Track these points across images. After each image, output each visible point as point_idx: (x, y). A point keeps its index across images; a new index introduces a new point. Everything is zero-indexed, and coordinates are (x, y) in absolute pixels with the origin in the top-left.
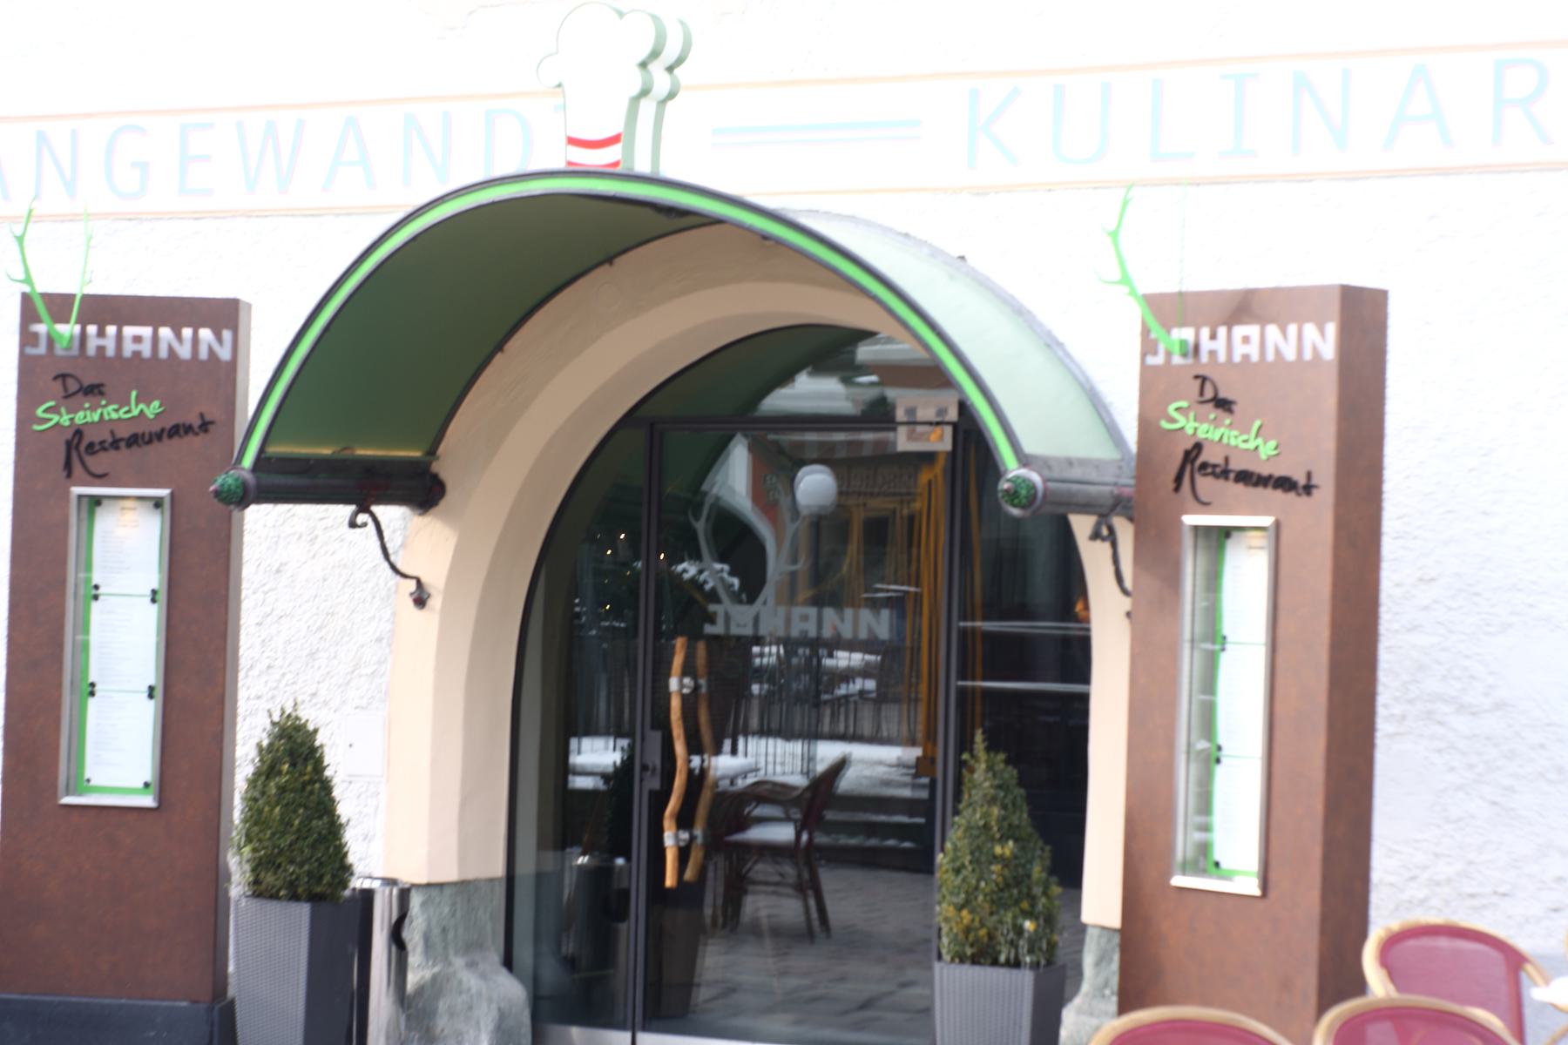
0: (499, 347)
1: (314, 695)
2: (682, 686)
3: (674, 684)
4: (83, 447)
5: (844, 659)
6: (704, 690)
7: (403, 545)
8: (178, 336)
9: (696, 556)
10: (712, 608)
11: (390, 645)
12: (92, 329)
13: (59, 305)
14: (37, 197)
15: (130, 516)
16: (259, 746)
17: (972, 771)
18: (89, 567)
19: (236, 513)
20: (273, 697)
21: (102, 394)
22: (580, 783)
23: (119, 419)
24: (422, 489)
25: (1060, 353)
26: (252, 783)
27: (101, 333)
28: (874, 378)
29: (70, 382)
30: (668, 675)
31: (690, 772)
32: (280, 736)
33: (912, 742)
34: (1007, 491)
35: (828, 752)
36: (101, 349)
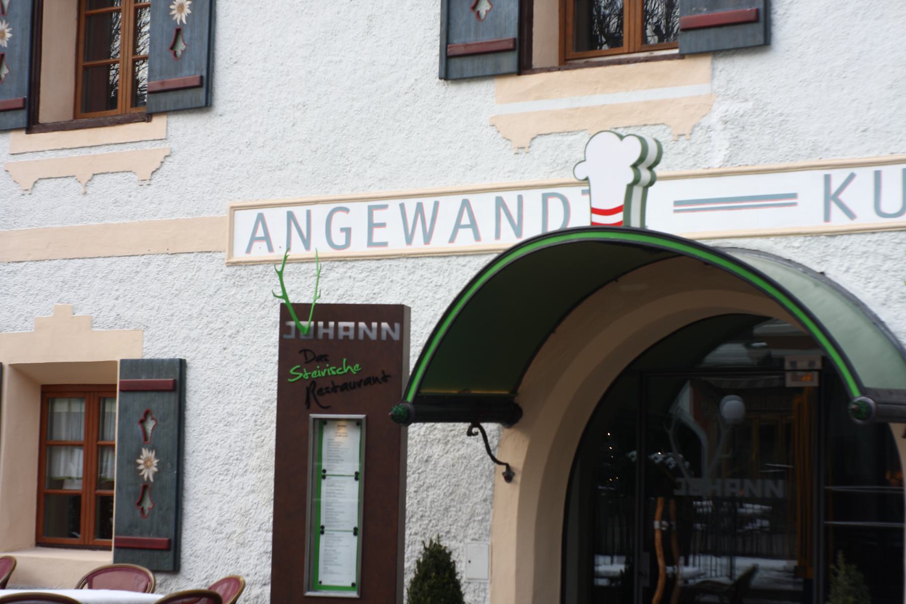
0: (552, 330)
1: (448, 532)
2: (661, 525)
3: (657, 524)
4: (316, 392)
5: (750, 509)
6: (674, 528)
7: (498, 445)
8: (369, 327)
9: (667, 449)
10: (679, 480)
11: (491, 503)
12: (321, 324)
13: (302, 310)
14: (288, 249)
15: (342, 431)
16: (418, 562)
17: (836, 575)
18: (319, 458)
19: (403, 428)
20: (425, 534)
21: (327, 360)
22: (602, 582)
23: (337, 375)
24: (509, 415)
25: (882, 328)
26: (414, 583)
27: (326, 326)
28: (764, 344)
29: (309, 354)
30: (654, 519)
31: (667, 575)
32: (431, 556)
33: (791, 557)
34: (853, 410)
35: (743, 563)
36: (326, 335)
